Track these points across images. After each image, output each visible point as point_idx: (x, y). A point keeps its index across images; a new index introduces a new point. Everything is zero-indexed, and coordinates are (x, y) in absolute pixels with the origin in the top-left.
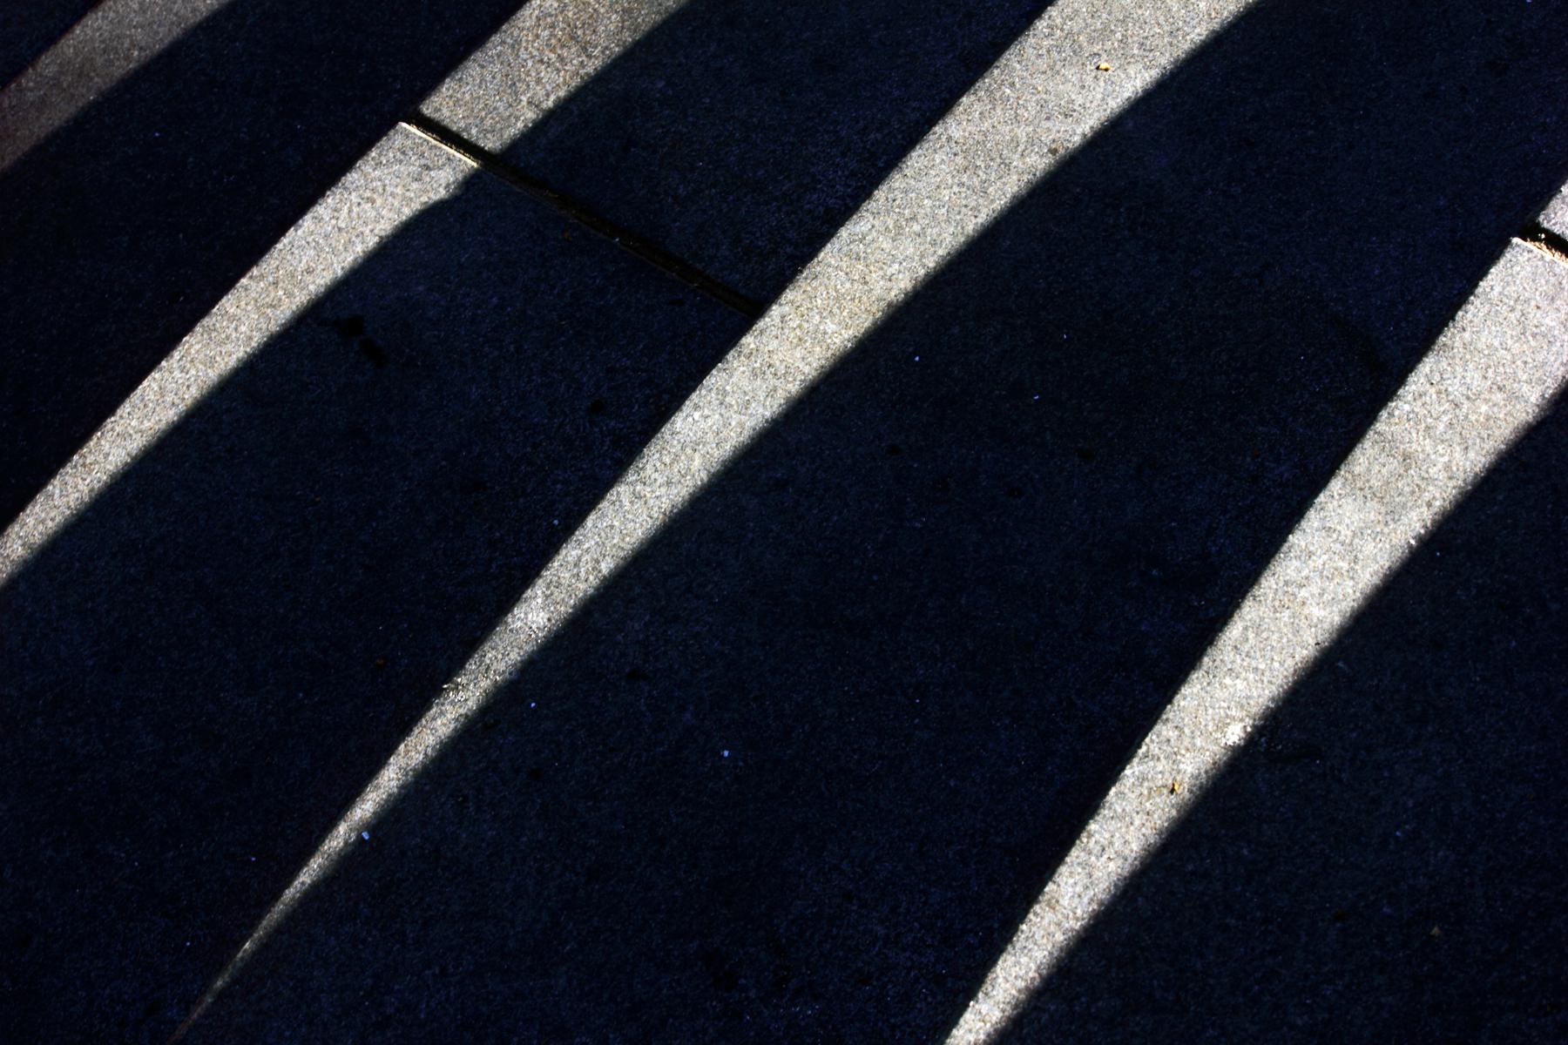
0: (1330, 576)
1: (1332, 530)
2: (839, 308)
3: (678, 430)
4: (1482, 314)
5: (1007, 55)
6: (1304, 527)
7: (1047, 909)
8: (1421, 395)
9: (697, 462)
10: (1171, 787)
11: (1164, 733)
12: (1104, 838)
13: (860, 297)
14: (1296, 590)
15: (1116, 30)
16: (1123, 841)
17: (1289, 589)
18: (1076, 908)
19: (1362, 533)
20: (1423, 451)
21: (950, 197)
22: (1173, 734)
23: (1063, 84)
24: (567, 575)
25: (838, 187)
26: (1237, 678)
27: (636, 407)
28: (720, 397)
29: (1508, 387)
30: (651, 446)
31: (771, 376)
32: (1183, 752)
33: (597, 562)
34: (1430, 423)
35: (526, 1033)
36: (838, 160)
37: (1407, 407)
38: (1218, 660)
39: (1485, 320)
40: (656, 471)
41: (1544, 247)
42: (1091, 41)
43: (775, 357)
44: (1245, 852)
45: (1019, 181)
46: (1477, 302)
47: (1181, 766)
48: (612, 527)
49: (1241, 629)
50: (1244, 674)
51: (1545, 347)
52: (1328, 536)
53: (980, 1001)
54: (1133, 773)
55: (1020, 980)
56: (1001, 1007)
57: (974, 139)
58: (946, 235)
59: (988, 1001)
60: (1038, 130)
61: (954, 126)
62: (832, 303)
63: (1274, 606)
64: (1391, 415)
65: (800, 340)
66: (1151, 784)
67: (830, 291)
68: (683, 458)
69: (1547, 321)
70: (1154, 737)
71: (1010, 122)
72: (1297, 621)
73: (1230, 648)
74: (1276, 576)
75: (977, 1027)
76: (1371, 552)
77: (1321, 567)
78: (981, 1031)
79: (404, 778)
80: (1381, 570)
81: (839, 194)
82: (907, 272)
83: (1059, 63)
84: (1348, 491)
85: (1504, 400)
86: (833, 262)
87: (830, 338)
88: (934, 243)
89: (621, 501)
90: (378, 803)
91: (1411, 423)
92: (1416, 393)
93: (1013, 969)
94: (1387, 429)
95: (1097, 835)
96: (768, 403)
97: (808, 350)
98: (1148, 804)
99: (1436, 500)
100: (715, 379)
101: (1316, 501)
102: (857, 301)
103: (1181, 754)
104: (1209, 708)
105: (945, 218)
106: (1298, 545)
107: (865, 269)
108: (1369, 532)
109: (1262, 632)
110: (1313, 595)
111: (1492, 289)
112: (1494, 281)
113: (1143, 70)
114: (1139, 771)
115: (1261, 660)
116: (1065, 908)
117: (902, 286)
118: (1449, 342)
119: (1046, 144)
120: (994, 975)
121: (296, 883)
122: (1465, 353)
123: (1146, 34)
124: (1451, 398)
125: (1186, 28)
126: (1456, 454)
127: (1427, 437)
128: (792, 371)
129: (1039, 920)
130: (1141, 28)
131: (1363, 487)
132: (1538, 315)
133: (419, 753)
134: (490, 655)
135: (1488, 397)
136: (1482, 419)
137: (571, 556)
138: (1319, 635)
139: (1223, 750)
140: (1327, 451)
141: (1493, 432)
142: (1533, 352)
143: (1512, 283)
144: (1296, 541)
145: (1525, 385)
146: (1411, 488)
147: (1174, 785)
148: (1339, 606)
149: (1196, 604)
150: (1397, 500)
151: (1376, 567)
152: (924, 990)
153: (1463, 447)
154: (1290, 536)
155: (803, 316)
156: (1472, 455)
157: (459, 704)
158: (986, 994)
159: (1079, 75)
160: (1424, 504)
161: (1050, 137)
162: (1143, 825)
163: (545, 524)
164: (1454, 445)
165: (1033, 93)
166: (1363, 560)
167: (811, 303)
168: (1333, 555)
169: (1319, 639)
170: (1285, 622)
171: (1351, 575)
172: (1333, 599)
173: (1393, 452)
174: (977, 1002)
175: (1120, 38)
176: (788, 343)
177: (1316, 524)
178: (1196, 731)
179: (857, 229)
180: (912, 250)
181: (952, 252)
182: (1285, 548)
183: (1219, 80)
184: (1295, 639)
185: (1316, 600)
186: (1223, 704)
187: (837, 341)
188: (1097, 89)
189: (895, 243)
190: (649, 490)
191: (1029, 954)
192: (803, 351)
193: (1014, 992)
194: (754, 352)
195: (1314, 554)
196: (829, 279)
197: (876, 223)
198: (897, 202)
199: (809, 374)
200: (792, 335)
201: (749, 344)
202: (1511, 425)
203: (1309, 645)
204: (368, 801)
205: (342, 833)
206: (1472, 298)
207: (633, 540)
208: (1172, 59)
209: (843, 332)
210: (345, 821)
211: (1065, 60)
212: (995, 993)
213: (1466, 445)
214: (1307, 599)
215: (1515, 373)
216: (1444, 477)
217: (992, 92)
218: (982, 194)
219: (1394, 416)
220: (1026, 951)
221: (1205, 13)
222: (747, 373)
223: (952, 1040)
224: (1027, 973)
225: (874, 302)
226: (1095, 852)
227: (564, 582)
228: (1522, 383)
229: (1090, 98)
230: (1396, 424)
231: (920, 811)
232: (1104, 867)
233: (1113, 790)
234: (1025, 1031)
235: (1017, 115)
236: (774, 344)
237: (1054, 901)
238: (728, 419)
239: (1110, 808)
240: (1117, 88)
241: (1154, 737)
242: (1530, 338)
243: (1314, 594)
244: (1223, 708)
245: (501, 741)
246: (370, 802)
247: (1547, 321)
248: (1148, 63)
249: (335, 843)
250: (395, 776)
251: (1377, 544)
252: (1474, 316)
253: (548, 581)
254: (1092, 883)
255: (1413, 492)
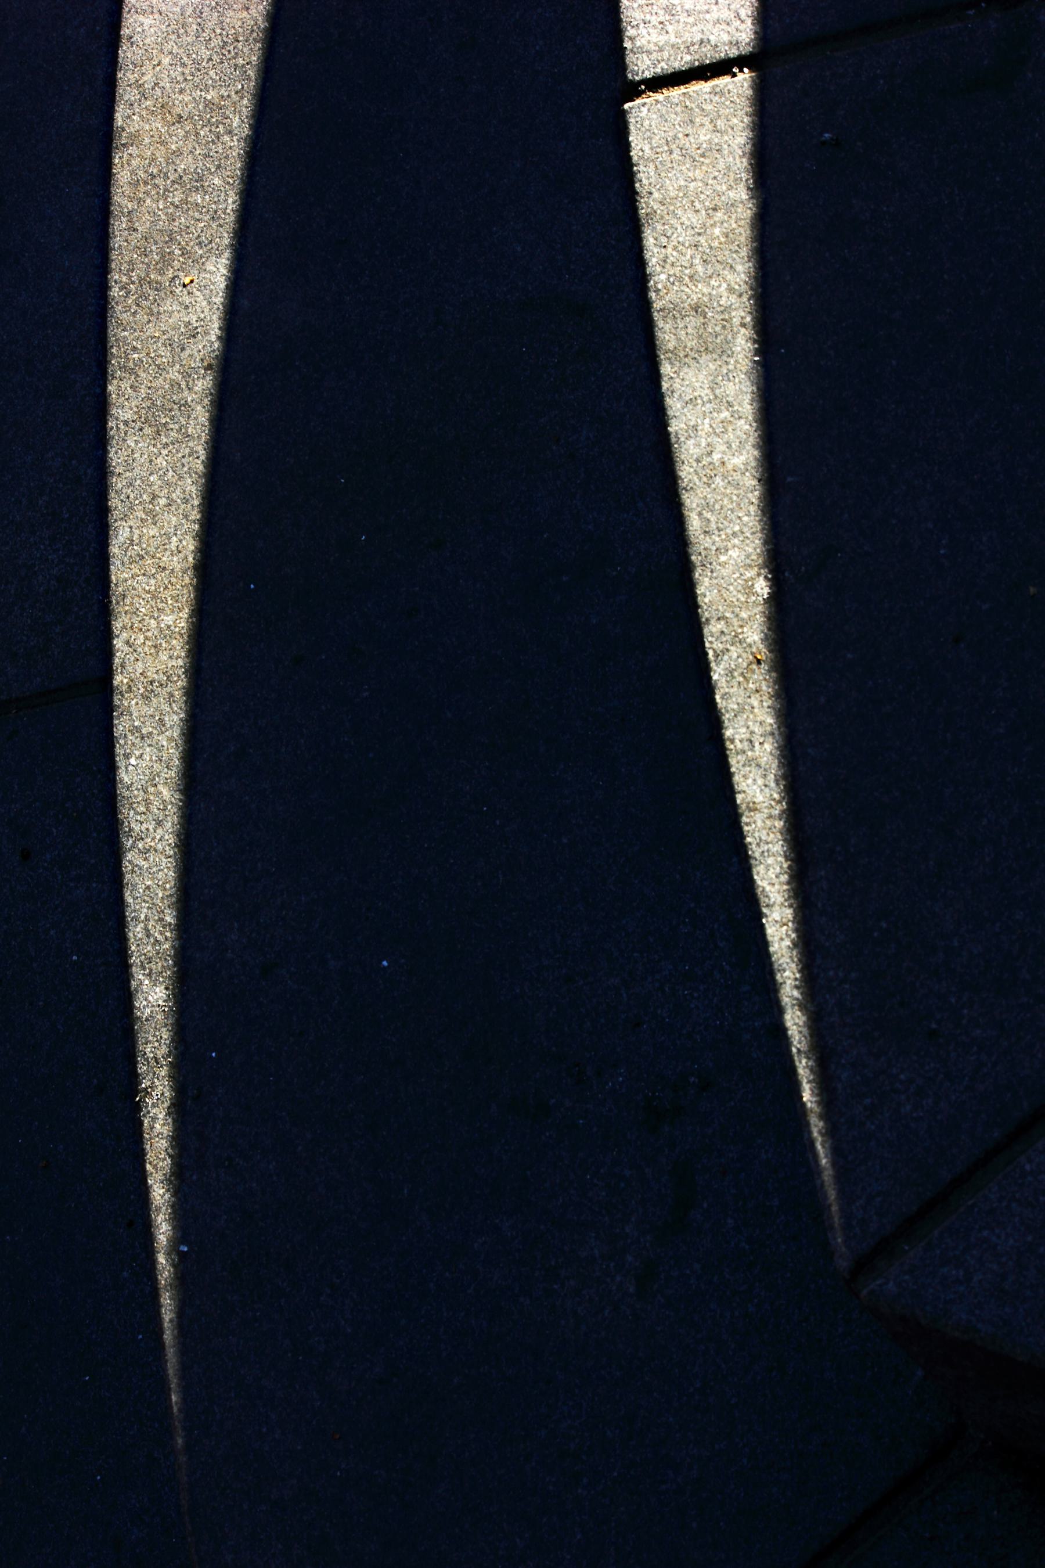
0: (723, 430)
1: (694, 399)
2: (162, 602)
3: (129, 783)
4: (653, 173)
5: (110, 332)
6: (672, 414)
7: (752, 814)
8: (665, 261)
9: (166, 793)
10: (755, 660)
11: (714, 630)
12: (744, 734)
13: (170, 581)
14: (709, 459)
15: (172, 249)
16: (758, 724)
17: (704, 463)
18: (771, 795)
19: (717, 384)
20: (703, 295)
21: (166, 461)
22: (721, 626)
23: (170, 317)
24: (149, 948)
25: (50, 557)
26: (727, 550)
27: (54, 830)
28: (136, 735)
29: (720, 204)
30: (121, 810)
31: (159, 689)
32: (740, 630)
33: (161, 920)
34: (690, 273)
35: (434, 1274)
36: (32, 539)
37: (663, 277)
38: (702, 551)
39: (659, 175)
40: (142, 823)
41: (651, 94)
42: (161, 272)
43: (149, 674)
44: (849, 656)
45: (204, 407)
46: (641, 168)
47: (748, 640)
48: (148, 888)
49: (697, 517)
50: (729, 544)
51: (718, 156)
52: (695, 406)
53: (768, 914)
54: (719, 674)
55: (781, 876)
56: (786, 904)
57: (144, 408)
58: (189, 488)
59: (774, 909)
60: (184, 362)
61: (120, 412)
62: (153, 603)
63: (705, 483)
64: (657, 291)
65: (155, 647)
66: (740, 671)
67: (144, 596)
68: (152, 798)
69: (702, 138)
70: (710, 639)
71: (158, 375)
72: (730, 479)
73: (702, 536)
74: (686, 462)
75: (784, 932)
76: (736, 390)
77: (711, 430)
78: (790, 933)
79: (171, 1186)
80: (754, 396)
81: (56, 561)
82: (186, 537)
83: (152, 306)
84: (678, 365)
85: (725, 214)
86: (127, 576)
87: (175, 627)
88: (186, 501)
89: (137, 865)
90: (169, 1220)
91: (676, 284)
92: (660, 262)
93: (770, 873)
94: (664, 302)
95: (737, 736)
96: (176, 709)
97: (168, 649)
98: (751, 685)
99: (745, 318)
100: (121, 726)
101: (663, 391)
102: (170, 586)
103: (740, 634)
104: (728, 587)
105: (176, 477)
106: (681, 430)
107: (154, 560)
108: (720, 378)
109: (713, 506)
110: (724, 453)
111: (643, 151)
112: (639, 145)
113: (218, 260)
114: (723, 670)
115: (732, 525)
116: (764, 802)
117: (192, 548)
118: (649, 210)
119: (199, 367)
120: (761, 889)
121: (166, 1325)
122: (667, 208)
123: (196, 234)
124: (687, 245)
125: (220, 206)
126: (729, 277)
127: (696, 283)
128: (171, 672)
129: (754, 826)
130: (188, 233)
131: (686, 353)
132: (692, 141)
133: (165, 1159)
134: (149, 1050)
135: (712, 222)
136: (723, 240)
137: (138, 933)
138: (755, 474)
139: (766, 605)
140: (604, 395)
141: (739, 241)
142: (713, 167)
143: (652, 136)
144: (677, 428)
145: (730, 192)
146: (720, 326)
147: (756, 657)
148: (749, 444)
149: (615, 573)
150: (718, 341)
151: (749, 397)
152: (686, 992)
153: (728, 268)
154: (669, 428)
155: (141, 630)
156: (739, 268)
157: (160, 1102)
158: (768, 906)
159: (176, 302)
160: (740, 328)
161: (197, 360)
162: (762, 701)
163: (68, 966)
164: (721, 272)
165: (155, 342)
166: (735, 400)
167: (138, 616)
168: (711, 415)
169: (758, 476)
170: (723, 486)
171: (737, 416)
172: (740, 442)
173: (683, 313)
174: (766, 916)
175: (180, 252)
176: (149, 657)
177: (679, 406)
178: (735, 609)
179: (121, 539)
180: (174, 519)
181: (204, 495)
182: (673, 440)
183: (279, 220)
184: (741, 491)
185: (729, 453)
186: (735, 576)
187: (183, 624)
188: (198, 300)
189: (158, 525)
190: (150, 840)
191: (770, 854)
192: (165, 653)
193: (785, 887)
194: (131, 683)
195: (697, 426)
196: (135, 589)
197: (131, 523)
198: (132, 496)
199: (185, 664)
200: (146, 649)
201: (122, 682)
202: (747, 226)
203: (755, 486)
204: (161, 1224)
205: (164, 1262)
206: (635, 168)
207: (173, 883)
208: (231, 235)
209: (181, 615)
210: (158, 1252)
211: (155, 301)
212: (773, 900)
213: (729, 266)
214: (723, 458)
215: (714, 191)
216: (735, 299)
217: (125, 367)
218: (186, 439)
219: (660, 290)
220: (766, 854)
221: (224, 185)
222: (140, 702)
223: (775, 956)
224: (781, 867)
225: (183, 576)
226: (746, 748)
227: (151, 954)
228: (726, 193)
229: (199, 310)
230: (667, 294)
231: (561, 878)
232: (763, 752)
233: (718, 697)
234: (820, 905)
235: (158, 366)
236: (140, 667)
237: (751, 805)
238: (157, 744)
239: (727, 711)
240: (212, 287)
241: (710, 639)
242: (702, 159)
243: (725, 451)
244: (739, 578)
245: (216, 1099)
246: (164, 1223)
247: (702, 138)
248: (217, 252)
249: (166, 1273)
250: (164, 1190)
251: (734, 381)
252: (648, 178)
253: (139, 964)
254: (765, 770)
255: (724, 327)
